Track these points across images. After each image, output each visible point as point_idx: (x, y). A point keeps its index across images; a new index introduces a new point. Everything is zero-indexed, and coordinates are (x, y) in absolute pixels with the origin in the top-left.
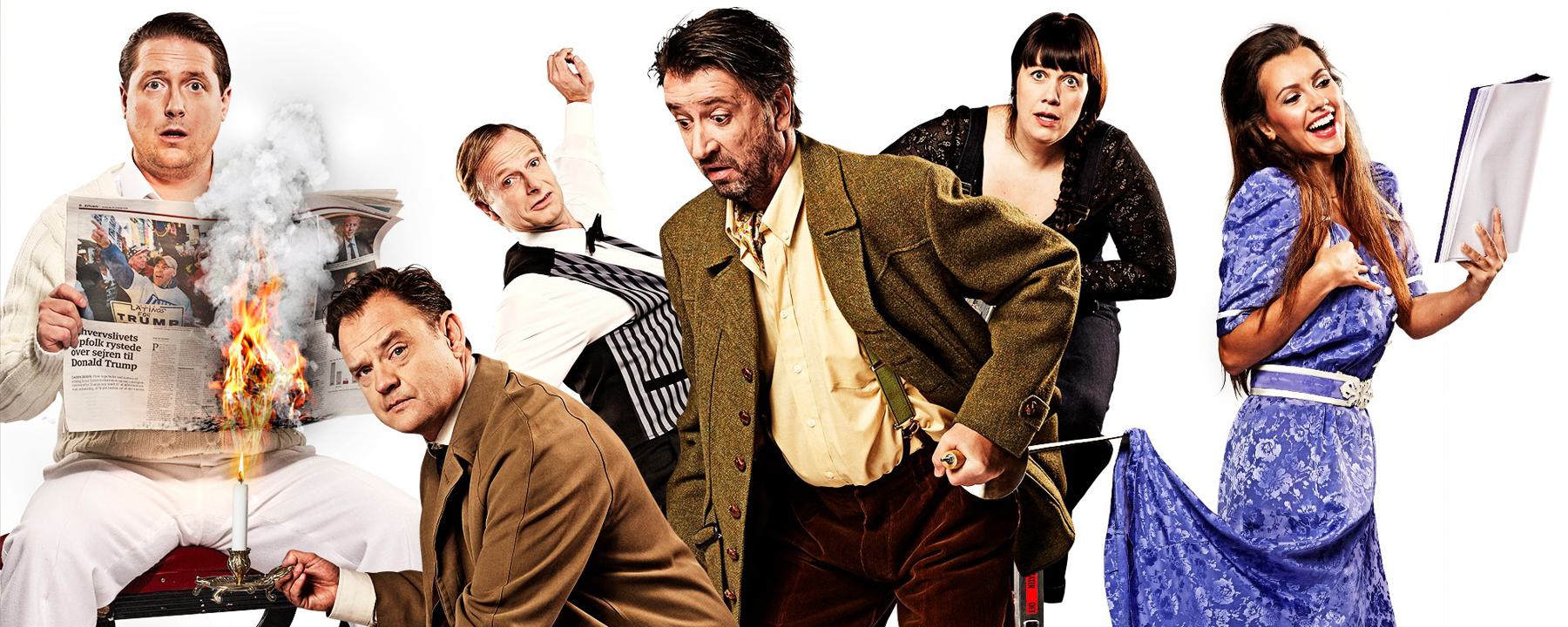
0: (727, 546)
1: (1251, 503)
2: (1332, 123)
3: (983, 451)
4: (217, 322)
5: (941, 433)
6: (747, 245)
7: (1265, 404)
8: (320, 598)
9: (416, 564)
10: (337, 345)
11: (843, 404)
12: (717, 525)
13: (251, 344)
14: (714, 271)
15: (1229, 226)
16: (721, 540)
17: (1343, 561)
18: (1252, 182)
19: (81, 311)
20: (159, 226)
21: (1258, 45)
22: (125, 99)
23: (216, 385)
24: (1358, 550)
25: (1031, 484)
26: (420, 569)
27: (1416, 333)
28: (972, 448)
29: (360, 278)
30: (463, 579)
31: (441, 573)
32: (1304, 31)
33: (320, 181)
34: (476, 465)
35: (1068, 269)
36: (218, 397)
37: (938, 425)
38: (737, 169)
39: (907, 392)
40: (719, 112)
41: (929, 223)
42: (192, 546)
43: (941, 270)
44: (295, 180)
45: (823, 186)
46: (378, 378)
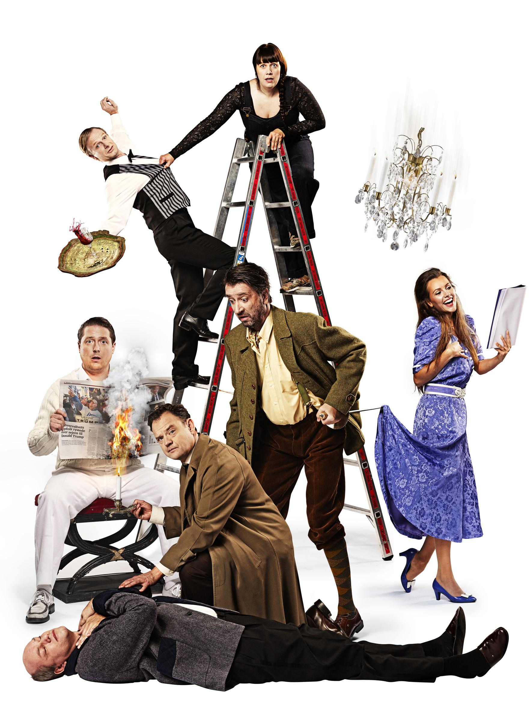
0: (247, 445)
1: (424, 430)
2: (452, 301)
3: (334, 413)
4: (111, 422)
5: (319, 407)
6: (253, 343)
7: (429, 397)
8: (145, 516)
9: (179, 505)
10: (151, 430)
11: (286, 397)
12: (243, 438)
13: (122, 430)
14: (242, 352)
15: (417, 336)
16: (245, 443)
17: (456, 450)
18: (425, 321)
19: (65, 418)
20: (91, 389)
21: (427, 275)
22: (79, 346)
23: (110, 443)
24: (460, 446)
25: (350, 424)
26: (179, 506)
27: (480, 373)
28: (330, 412)
29: (159, 407)
30: (194, 509)
31: (186, 507)
32: (443, 270)
33: (146, 374)
34: (198, 470)
35: (362, 351)
36: (111, 447)
37: (318, 404)
38: (250, 317)
39: (308, 393)
40: (244, 298)
41: (315, 335)
42: (102, 498)
43: (319, 351)
44: (137, 374)
45: (279, 323)
46: (165, 441)
